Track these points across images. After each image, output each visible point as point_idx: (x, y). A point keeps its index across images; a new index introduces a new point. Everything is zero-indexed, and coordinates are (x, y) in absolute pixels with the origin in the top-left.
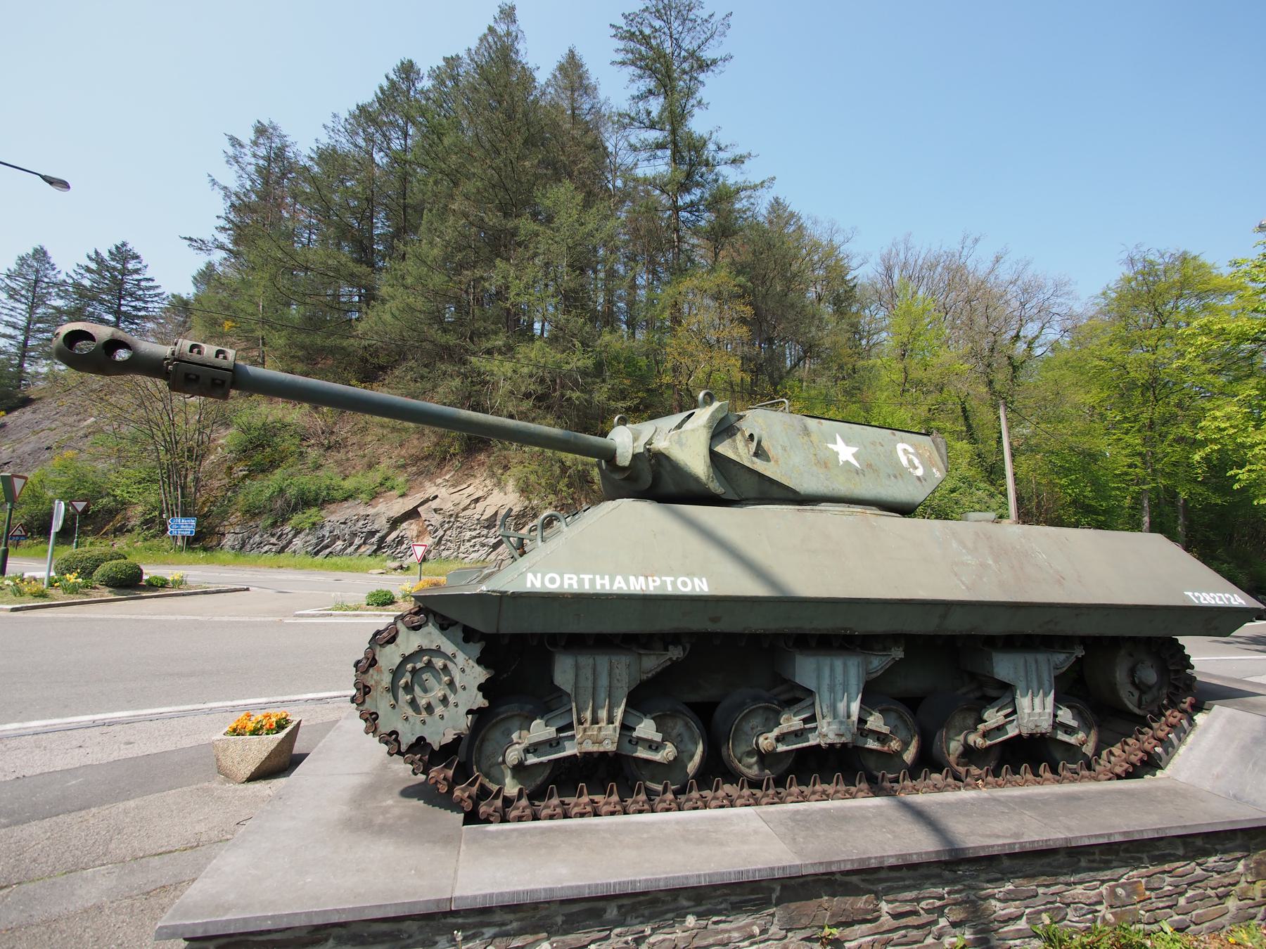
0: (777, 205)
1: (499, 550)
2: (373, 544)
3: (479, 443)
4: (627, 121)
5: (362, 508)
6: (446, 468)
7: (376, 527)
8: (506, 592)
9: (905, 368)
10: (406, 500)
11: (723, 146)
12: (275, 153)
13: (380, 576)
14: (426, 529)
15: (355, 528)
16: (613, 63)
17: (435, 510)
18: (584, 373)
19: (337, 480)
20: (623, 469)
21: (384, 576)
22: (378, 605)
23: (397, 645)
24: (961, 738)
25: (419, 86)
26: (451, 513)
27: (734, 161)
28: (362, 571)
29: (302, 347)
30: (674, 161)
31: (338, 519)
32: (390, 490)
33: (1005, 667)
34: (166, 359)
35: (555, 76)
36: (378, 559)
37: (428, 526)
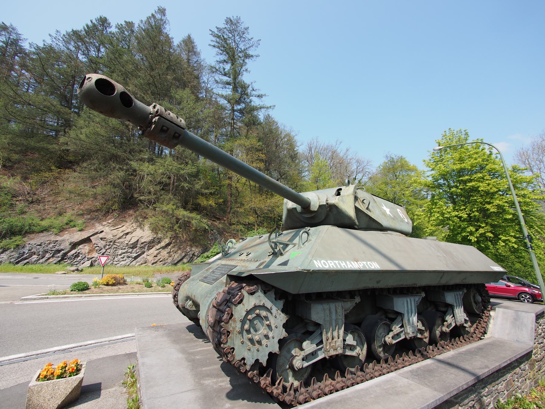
0: (268, 117)
1: (137, 259)
2: (58, 257)
3: (129, 205)
4: (214, 70)
5: (53, 237)
6: (109, 217)
7: (62, 247)
8: (310, 270)
9: (317, 186)
10: (83, 233)
11: (255, 89)
12: (11, 42)
13: (64, 275)
14: (94, 249)
15: (47, 248)
16: (210, 45)
17: (101, 239)
18: (191, 175)
19: (37, 221)
20: (314, 212)
21: (67, 275)
22: (79, 290)
23: (243, 305)
24: (439, 329)
25: (109, 30)
26: (111, 240)
27: (259, 96)
28: (50, 273)
29: (18, 145)
31: (36, 242)
32: (73, 227)
33: (450, 298)
34: (151, 114)
35: (181, 44)
36: (61, 265)
37: (96, 247)
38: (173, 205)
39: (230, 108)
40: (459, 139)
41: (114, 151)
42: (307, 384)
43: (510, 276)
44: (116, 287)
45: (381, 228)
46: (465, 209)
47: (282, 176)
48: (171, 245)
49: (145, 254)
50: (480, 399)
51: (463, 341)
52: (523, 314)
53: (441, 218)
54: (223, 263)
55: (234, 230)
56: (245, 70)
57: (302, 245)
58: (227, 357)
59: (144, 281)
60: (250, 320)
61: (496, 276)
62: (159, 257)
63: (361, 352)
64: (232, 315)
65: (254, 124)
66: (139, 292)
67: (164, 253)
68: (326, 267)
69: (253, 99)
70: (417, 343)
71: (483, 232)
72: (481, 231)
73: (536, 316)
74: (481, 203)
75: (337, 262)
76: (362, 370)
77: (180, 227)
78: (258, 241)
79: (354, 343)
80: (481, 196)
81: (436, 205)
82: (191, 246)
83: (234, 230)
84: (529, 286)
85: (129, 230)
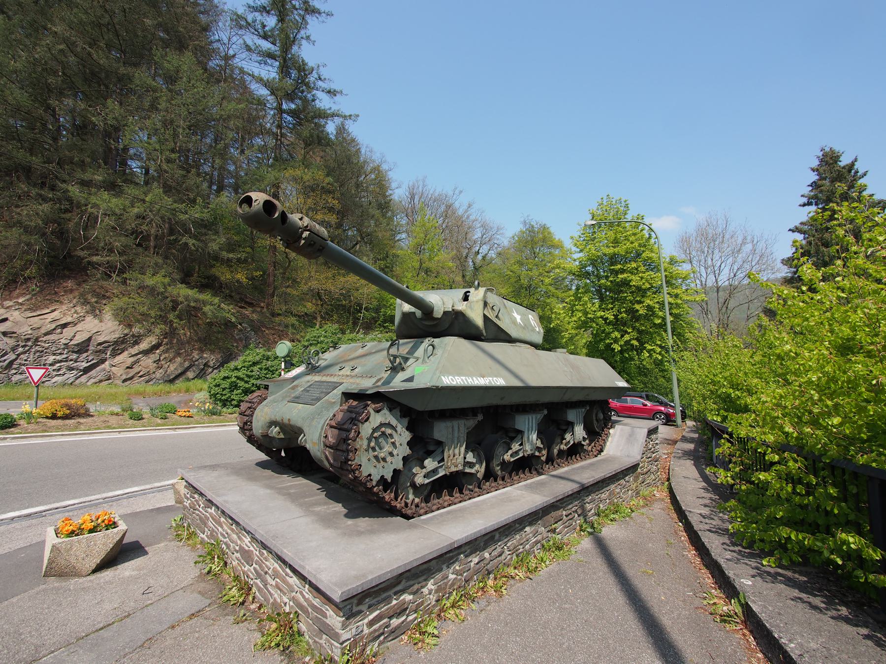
1: (91, 373)
4: (243, 23)
11: (322, 78)
20: (437, 319)
24: (558, 447)
26: (27, 337)
27: (329, 92)
30: (282, 72)
33: (571, 415)
34: (300, 228)
38: (165, 276)
39: (275, 105)
40: (617, 212)
41: (21, 155)
42: (427, 500)
43: (650, 393)
44: (73, 421)
45: (508, 339)
46: (612, 309)
47: (367, 238)
48: (162, 348)
49: (107, 363)
50: (582, 506)
51: (579, 459)
52: (638, 429)
53: (583, 319)
54: (317, 380)
55: (279, 325)
56: (304, 36)
57: (426, 358)
58: (354, 473)
59: (123, 410)
60: (375, 438)
61: (619, 392)
62: (136, 369)
63: (479, 470)
64: (359, 433)
65: (319, 143)
66: (119, 428)
67: (148, 362)
68: (454, 383)
69: (319, 94)
70: (534, 462)
71: (629, 339)
72: (627, 337)
73: (649, 432)
74: (631, 302)
75: (464, 378)
76: (479, 487)
77: (180, 317)
78: (361, 351)
79: (474, 461)
80: (632, 293)
81: (580, 301)
82: (201, 351)
83: (279, 325)
84: (666, 405)
85: (69, 319)
